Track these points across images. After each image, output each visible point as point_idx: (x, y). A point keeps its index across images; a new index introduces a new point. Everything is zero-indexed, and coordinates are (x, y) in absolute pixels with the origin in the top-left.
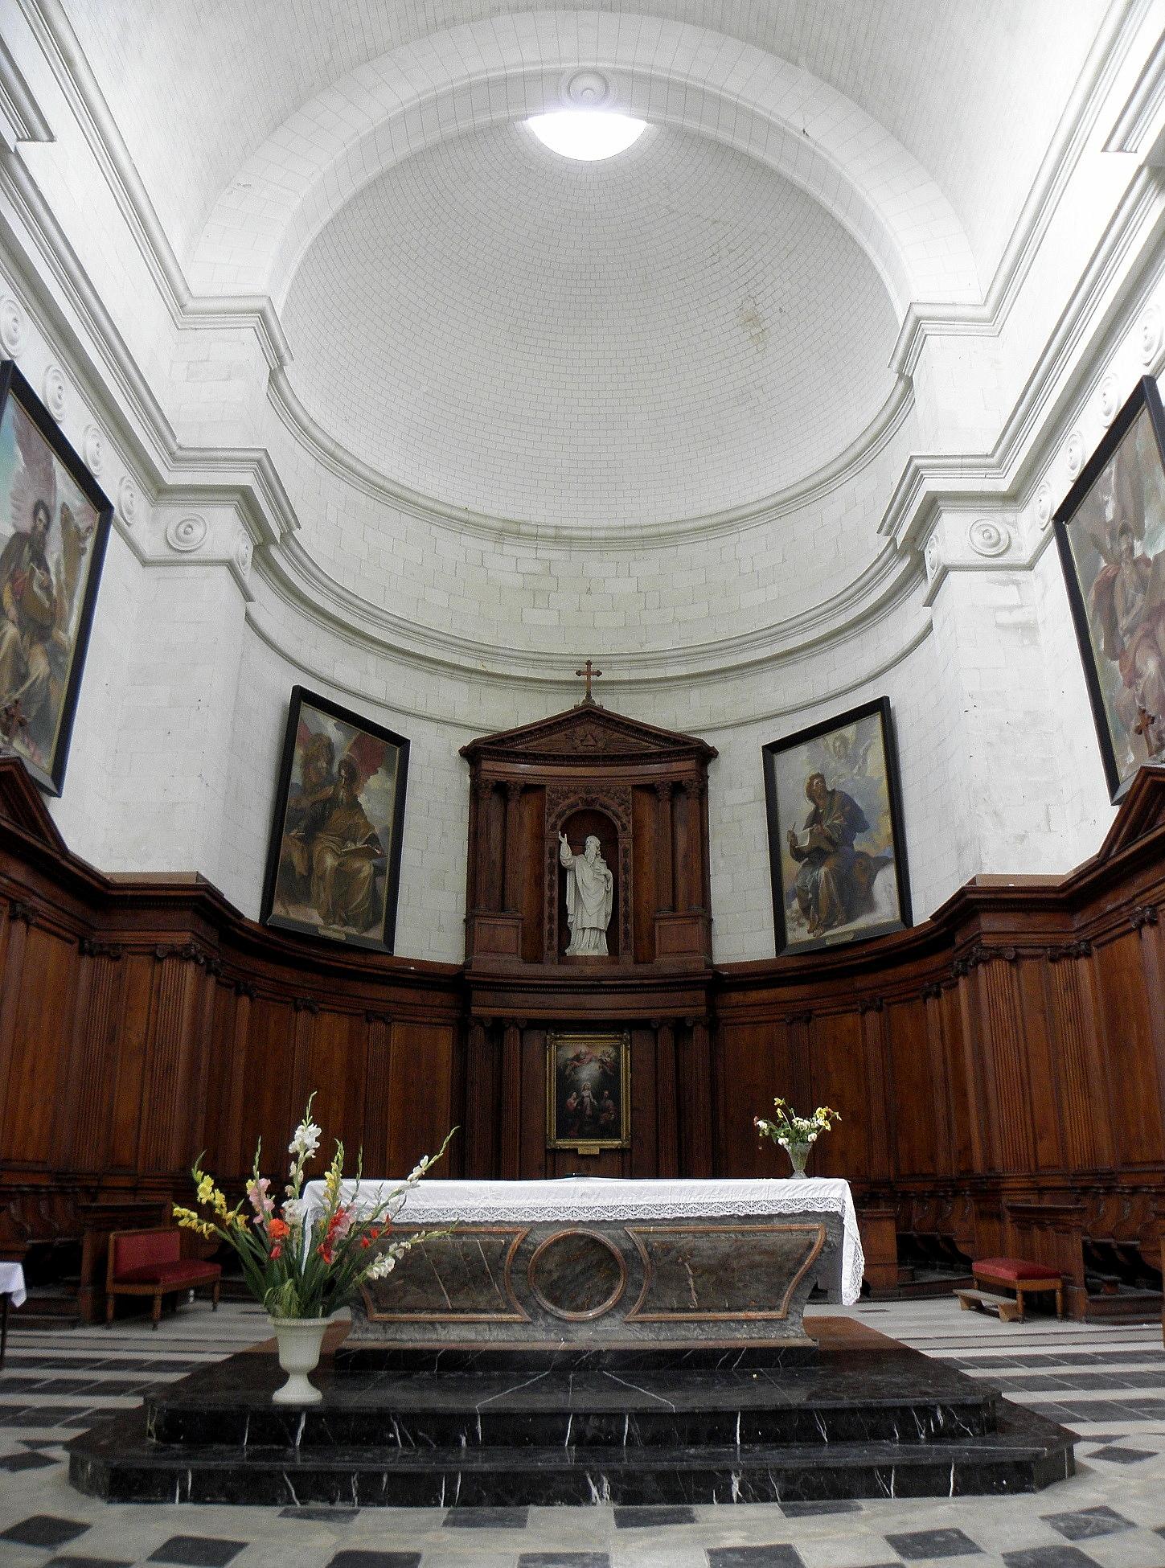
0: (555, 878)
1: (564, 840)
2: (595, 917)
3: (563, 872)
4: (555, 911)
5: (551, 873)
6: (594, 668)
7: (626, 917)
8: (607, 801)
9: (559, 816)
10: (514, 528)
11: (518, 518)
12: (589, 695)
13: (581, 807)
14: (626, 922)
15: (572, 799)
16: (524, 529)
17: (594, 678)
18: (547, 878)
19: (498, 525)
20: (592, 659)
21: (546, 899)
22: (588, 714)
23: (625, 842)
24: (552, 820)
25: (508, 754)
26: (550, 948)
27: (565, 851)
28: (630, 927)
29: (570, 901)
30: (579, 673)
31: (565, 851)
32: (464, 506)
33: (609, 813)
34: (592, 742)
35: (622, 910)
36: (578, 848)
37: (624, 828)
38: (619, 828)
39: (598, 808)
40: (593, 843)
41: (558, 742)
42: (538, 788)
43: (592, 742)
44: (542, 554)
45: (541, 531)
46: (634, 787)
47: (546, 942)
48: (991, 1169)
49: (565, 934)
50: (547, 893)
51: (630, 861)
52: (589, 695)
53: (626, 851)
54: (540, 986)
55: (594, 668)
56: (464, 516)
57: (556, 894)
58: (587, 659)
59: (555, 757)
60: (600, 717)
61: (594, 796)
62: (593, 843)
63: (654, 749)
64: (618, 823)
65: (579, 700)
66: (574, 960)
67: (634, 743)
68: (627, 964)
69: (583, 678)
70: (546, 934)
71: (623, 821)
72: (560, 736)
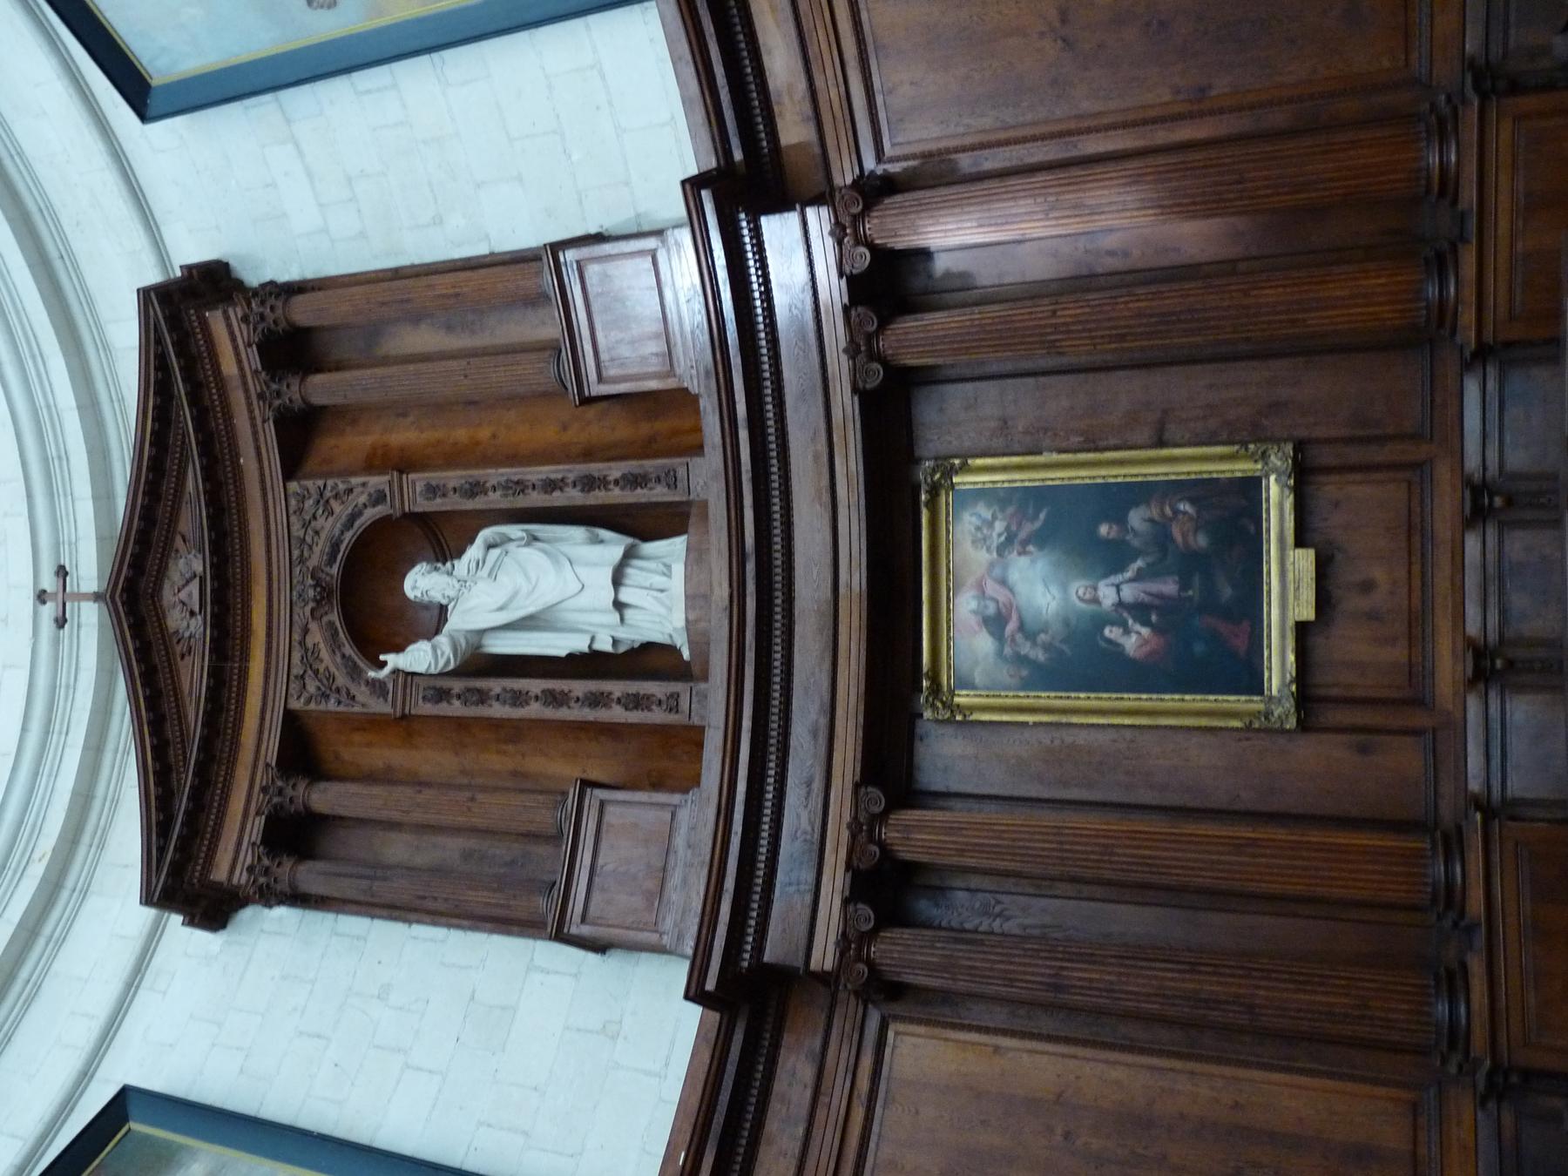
0: (496, 685)
1: (393, 660)
3: (481, 665)
4: (579, 687)
13: (335, 617)
15: (316, 637)
18: (498, 711)
21: (550, 713)
23: (415, 493)
27: (418, 657)
28: (616, 470)
37: (379, 498)
47: (657, 716)
62: (421, 583)
64: (371, 514)
70: (635, 717)
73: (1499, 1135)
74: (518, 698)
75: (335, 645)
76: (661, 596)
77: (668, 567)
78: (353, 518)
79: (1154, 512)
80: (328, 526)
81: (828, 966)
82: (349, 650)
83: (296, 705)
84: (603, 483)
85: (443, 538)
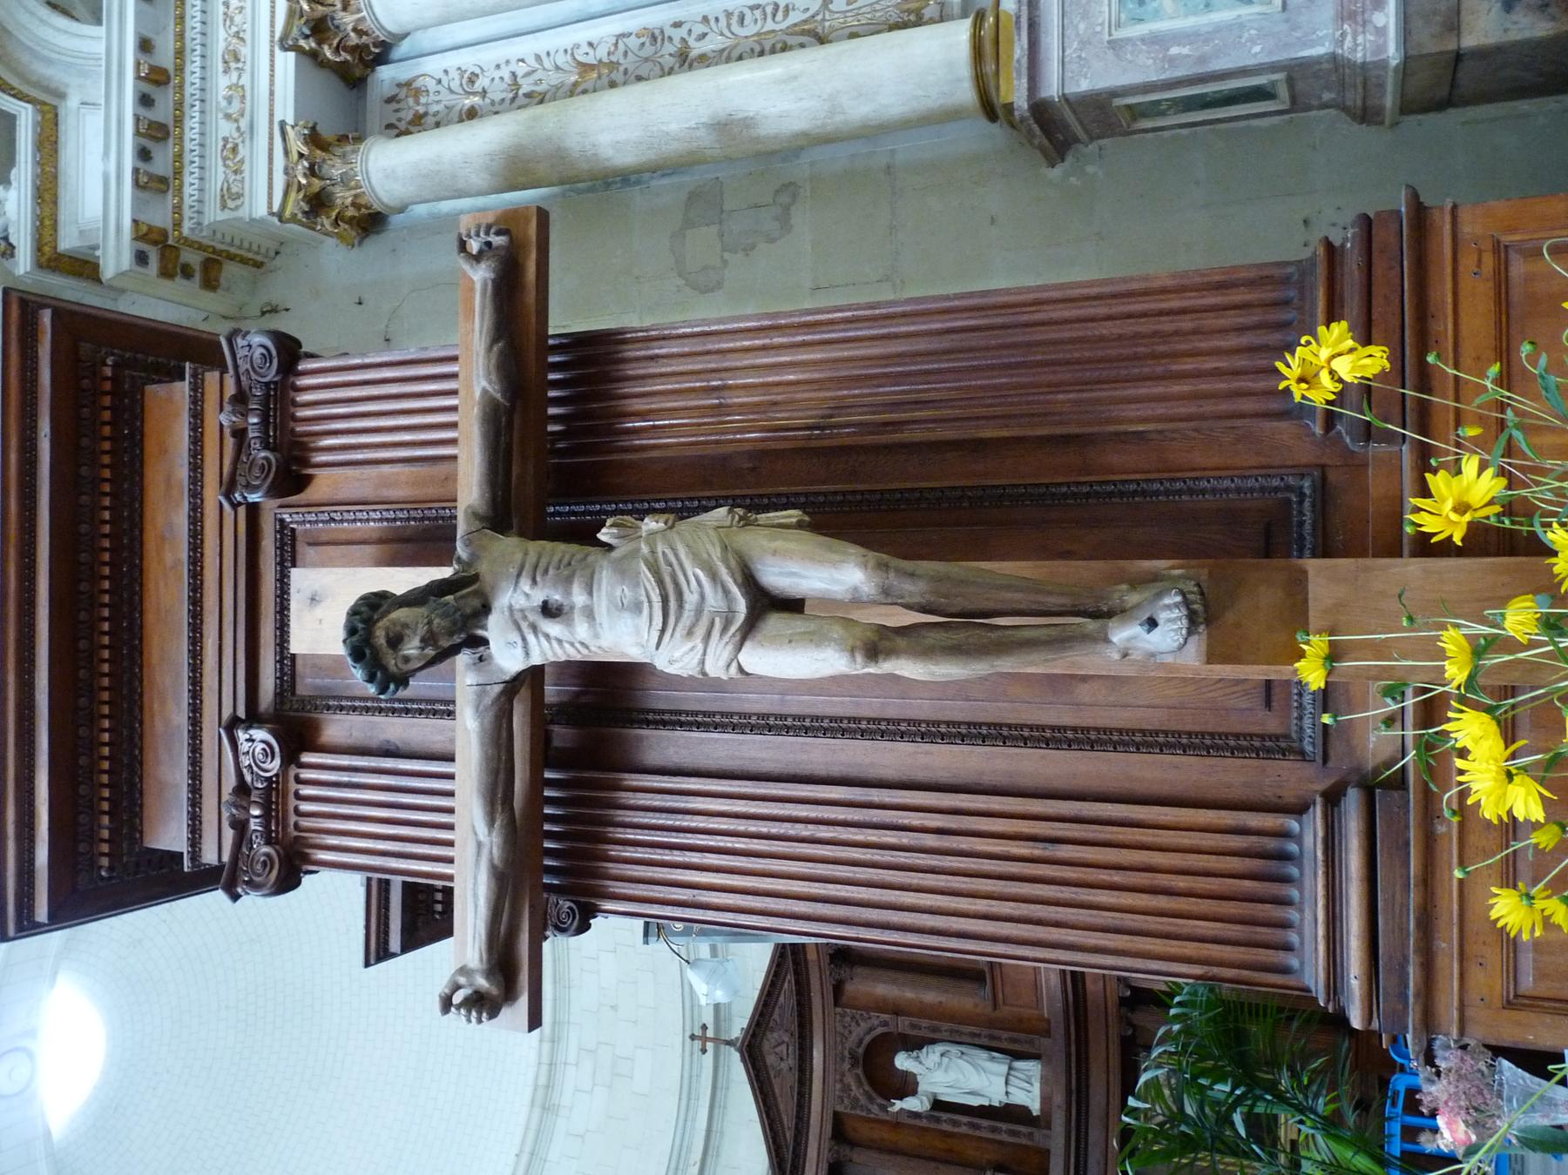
0: (945, 1116)
1: (899, 1105)
2: (992, 1078)
3: (938, 1105)
4: (985, 1123)
5: (938, 1120)
6: (698, 1032)
7: (992, 1037)
8: (853, 1038)
9: (871, 1099)
10: (540, 1093)
11: (529, 1091)
12: (729, 1043)
13: (859, 1071)
14: (999, 1039)
15: (850, 1079)
16: (542, 1080)
17: (710, 1033)
18: (946, 1127)
19: (537, 1111)
20: (688, 1034)
21: (971, 1132)
22: (752, 1050)
23: (903, 1025)
24: (875, 1109)
25: (796, 1155)
26: (1031, 1042)
27: (911, 1104)
28: (1005, 1035)
29: (975, 1102)
30: (704, 1051)
31: (911, 1104)
32: (513, 1158)
33: (868, 1039)
34: (784, 1047)
35: (985, 1041)
36: (907, 1085)
37: (885, 1024)
38: (884, 1030)
39: (861, 1051)
40: (903, 1062)
41: (784, 1088)
42: (837, 1117)
43: (784, 1047)
44: (572, 1058)
45: (545, 1059)
46: (836, 1005)
47: (1024, 1141)
48: (1340, 380)
49: (1011, 1114)
50: (964, 1129)
51: (925, 1023)
52: (729, 1043)
53: (913, 1026)
54: (1077, 1148)
55: (698, 1032)
56: (525, 1158)
57: (965, 1119)
58: (688, 1040)
59: (801, 1095)
60: (754, 1035)
61: (846, 1053)
62: (903, 1062)
63: (790, 977)
64: (880, 1030)
65: (736, 1056)
66: (1046, 1100)
67: (787, 997)
68: (1055, 1044)
69: (710, 1045)
70: (1011, 1140)
71: (876, 1024)
72: (776, 1083)
73: (1515, 952)
74: (955, 1123)
75: (860, 1084)
76: (1023, 1086)
77: (1030, 1077)
78: (871, 1029)
79: (1245, 1109)
80: (858, 1031)
81: (208, 375)
82: (867, 1088)
83: (839, 1108)
84: (999, 1039)
85: (914, 1044)
